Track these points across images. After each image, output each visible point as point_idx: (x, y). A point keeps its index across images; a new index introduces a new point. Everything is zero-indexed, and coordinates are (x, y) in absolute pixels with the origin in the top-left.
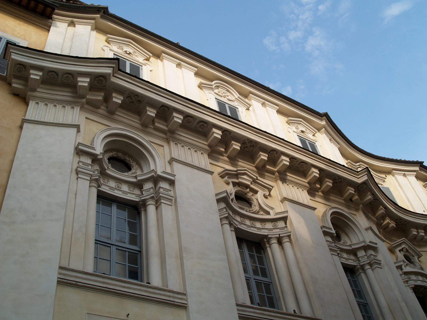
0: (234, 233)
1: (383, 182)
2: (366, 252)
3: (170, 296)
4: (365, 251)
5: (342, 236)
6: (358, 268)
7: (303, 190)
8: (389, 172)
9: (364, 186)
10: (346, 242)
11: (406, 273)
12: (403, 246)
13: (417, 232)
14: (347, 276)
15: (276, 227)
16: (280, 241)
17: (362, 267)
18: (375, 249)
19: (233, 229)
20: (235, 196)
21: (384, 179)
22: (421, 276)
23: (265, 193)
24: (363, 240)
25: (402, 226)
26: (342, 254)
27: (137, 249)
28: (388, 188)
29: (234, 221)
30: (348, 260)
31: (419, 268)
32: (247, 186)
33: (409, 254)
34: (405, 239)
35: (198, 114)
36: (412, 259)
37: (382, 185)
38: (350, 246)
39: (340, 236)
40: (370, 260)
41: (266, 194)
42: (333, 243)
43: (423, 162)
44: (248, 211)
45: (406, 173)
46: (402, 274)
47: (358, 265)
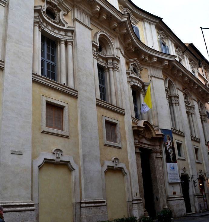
0: (40, 33)
3: (70, 91)
6: (106, 68)
8: (142, 19)
11: (131, 77)
16: (191, 113)
17: (108, 69)
18: (118, 61)
19: (41, 30)
20: (47, 10)
22: (138, 81)
23: (65, 12)
27: (55, 64)
28: (138, 28)
29: (42, 25)
32: (55, 6)
35: (116, 15)
37: (135, 25)
38: (105, 55)
39: (102, 49)
45: (151, 22)
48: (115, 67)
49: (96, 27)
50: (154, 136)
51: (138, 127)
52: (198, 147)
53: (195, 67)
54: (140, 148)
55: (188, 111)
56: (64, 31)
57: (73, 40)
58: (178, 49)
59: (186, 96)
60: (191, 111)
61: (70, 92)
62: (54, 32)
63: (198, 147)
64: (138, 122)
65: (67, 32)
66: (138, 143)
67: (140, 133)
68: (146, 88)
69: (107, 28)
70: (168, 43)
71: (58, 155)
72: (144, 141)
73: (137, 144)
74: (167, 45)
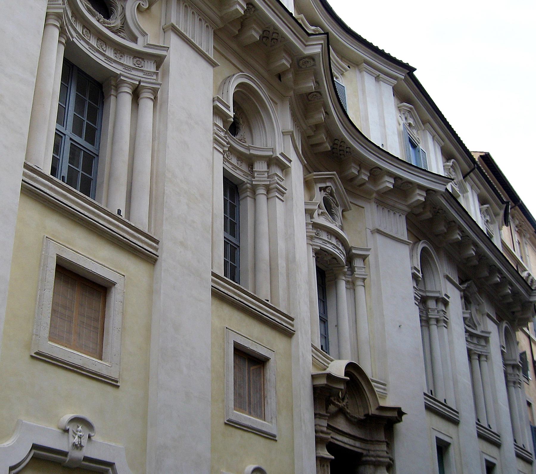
0: (62, 48)
1: (341, 74)
2: (268, 168)
4: (269, 166)
5: (241, 129)
6: (247, 188)
7: (207, 26)
9: (309, 63)
10: (244, 140)
11: (316, 226)
12: (328, 184)
13: (358, 172)
14: (225, 195)
15: (139, 67)
16: (479, 356)
17: (254, 189)
18: (284, 168)
19: (64, 41)
21: (345, 71)
24: (272, 147)
25: (341, 152)
26: (231, 156)
30: (236, 170)
31: (338, 226)
33: (332, 200)
34: (336, 174)
36: (333, 208)
38: (248, 148)
39: (238, 128)
40: (270, 181)
41: (143, 5)
42: (223, 131)
43: (415, 69)
44: (100, 21)
45: (382, 76)
46: (309, 223)
47: (248, 183)
48: (274, 186)
49: (227, 62)
50: (373, 411)
51: (329, 377)
52: (495, 459)
53: (492, 222)
54: (332, 447)
55: (472, 347)
56: (135, 57)
57: (160, 85)
58: (451, 164)
59: (467, 300)
60: (479, 349)
61: (134, 241)
62: (104, 55)
63: (495, 459)
64: (329, 364)
65: (143, 59)
66: (325, 429)
67: (332, 399)
68: (358, 263)
69: (262, 71)
70: (426, 142)
71: (80, 437)
72: (341, 424)
73: (322, 432)
74: (421, 146)
